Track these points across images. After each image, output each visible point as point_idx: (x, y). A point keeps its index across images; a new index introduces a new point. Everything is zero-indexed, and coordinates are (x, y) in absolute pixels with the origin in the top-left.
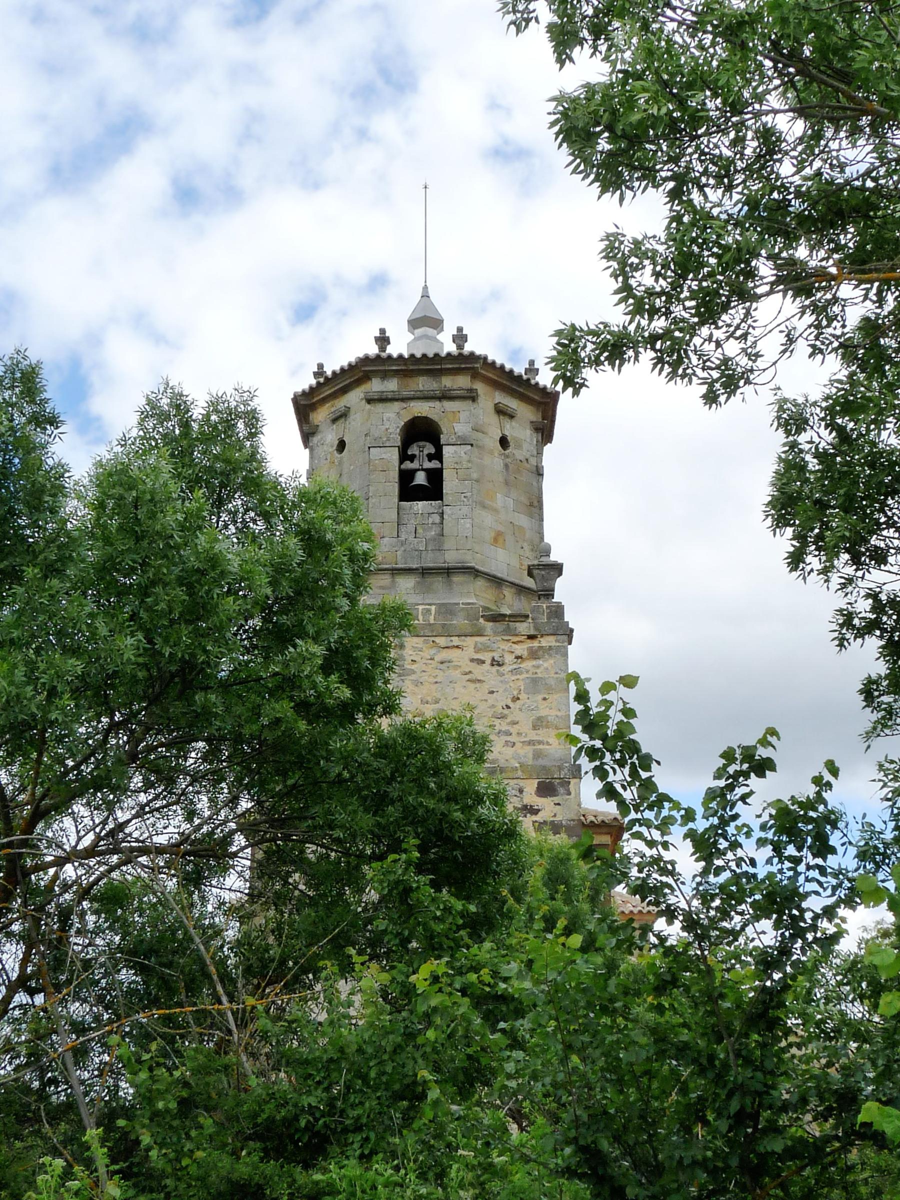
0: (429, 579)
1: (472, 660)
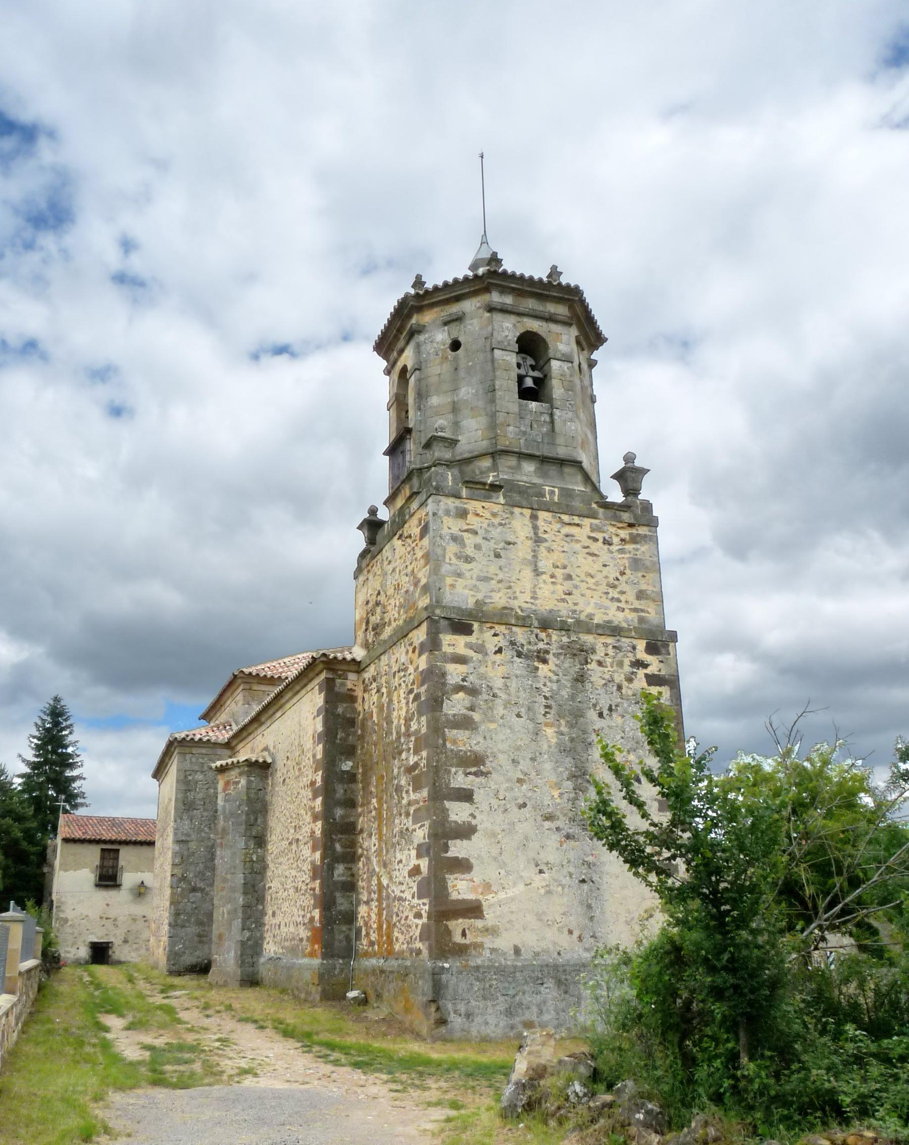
0: (547, 467)
1: (589, 537)
